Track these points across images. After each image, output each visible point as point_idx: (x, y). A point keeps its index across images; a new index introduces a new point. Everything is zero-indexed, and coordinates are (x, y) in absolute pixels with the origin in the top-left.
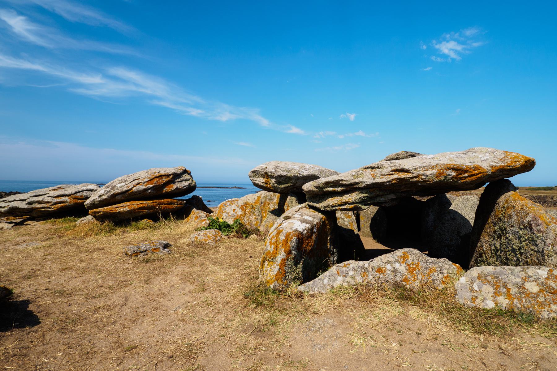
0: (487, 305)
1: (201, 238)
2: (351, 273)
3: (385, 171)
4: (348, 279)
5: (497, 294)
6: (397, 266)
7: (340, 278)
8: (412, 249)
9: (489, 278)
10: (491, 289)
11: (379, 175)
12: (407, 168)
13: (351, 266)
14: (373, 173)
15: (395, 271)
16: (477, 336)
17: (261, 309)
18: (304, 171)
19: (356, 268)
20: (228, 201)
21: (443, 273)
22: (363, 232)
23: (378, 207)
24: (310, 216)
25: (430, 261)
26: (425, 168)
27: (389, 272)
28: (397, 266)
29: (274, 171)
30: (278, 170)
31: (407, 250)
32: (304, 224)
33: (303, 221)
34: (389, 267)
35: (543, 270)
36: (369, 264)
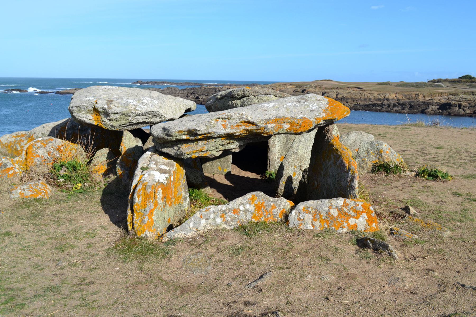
0: (307, 227)
1: (28, 193)
2: (212, 216)
3: (234, 122)
4: (210, 221)
5: (315, 219)
6: (248, 206)
7: (203, 222)
8: (258, 192)
9: (310, 209)
10: (311, 218)
11: (229, 126)
12: (252, 121)
13: (212, 210)
14: (224, 123)
15: (246, 211)
16: (263, 219)
17: (421, 119)
18: (142, 106)
19: (216, 211)
20: (38, 141)
21: (281, 209)
22: (174, 115)
23: (231, 155)
24: (166, 165)
25: (271, 200)
26: (267, 121)
27: (242, 212)
28: (248, 206)
29: (106, 107)
30: (111, 106)
31: (255, 193)
32: (163, 175)
33: (162, 171)
34: (241, 208)
35: (341, 200)
36: (226, 207)
